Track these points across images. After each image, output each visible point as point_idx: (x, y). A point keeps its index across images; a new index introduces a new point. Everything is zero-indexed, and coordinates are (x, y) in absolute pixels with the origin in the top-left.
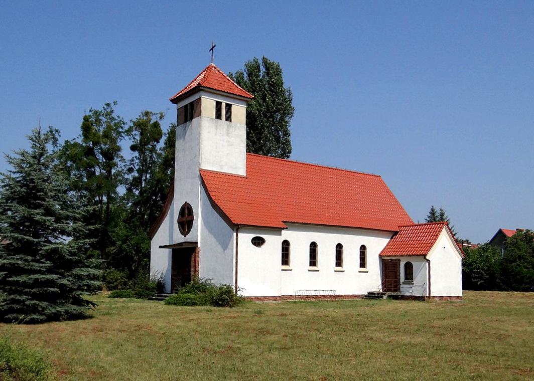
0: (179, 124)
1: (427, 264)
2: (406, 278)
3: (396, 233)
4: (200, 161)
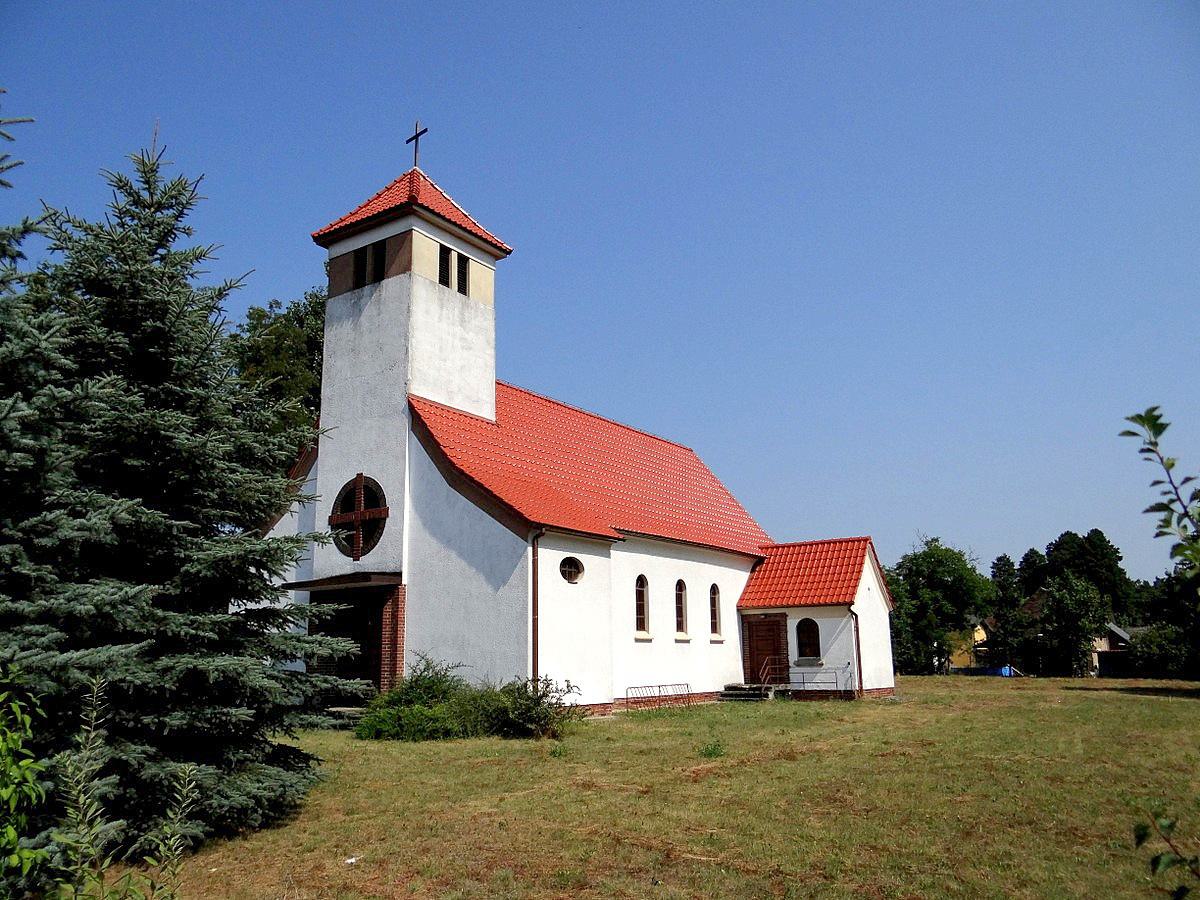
0: (333, 291)
1: (853, 623)
2: (801, 653)
3: (759, 561)
4: (409, 377)
